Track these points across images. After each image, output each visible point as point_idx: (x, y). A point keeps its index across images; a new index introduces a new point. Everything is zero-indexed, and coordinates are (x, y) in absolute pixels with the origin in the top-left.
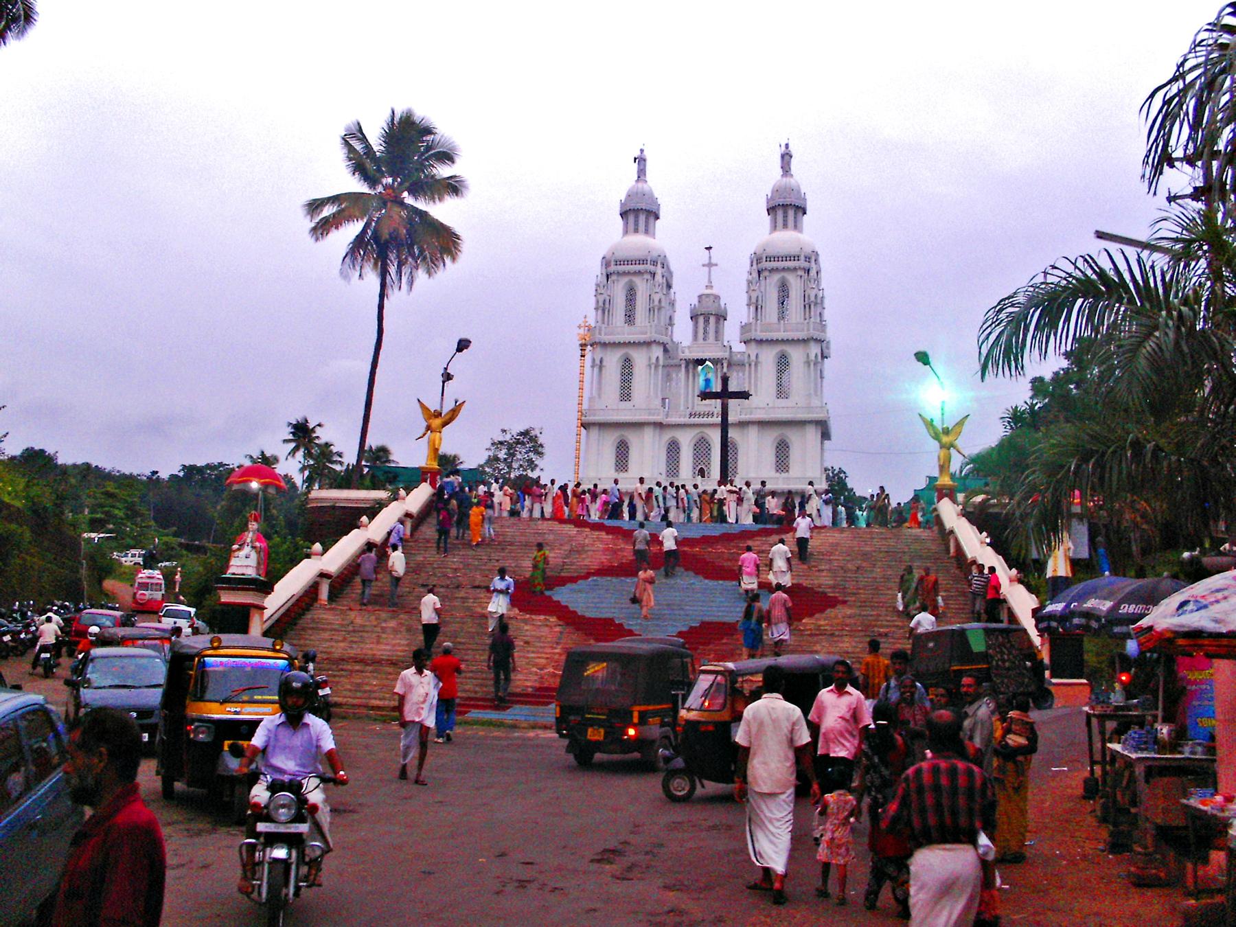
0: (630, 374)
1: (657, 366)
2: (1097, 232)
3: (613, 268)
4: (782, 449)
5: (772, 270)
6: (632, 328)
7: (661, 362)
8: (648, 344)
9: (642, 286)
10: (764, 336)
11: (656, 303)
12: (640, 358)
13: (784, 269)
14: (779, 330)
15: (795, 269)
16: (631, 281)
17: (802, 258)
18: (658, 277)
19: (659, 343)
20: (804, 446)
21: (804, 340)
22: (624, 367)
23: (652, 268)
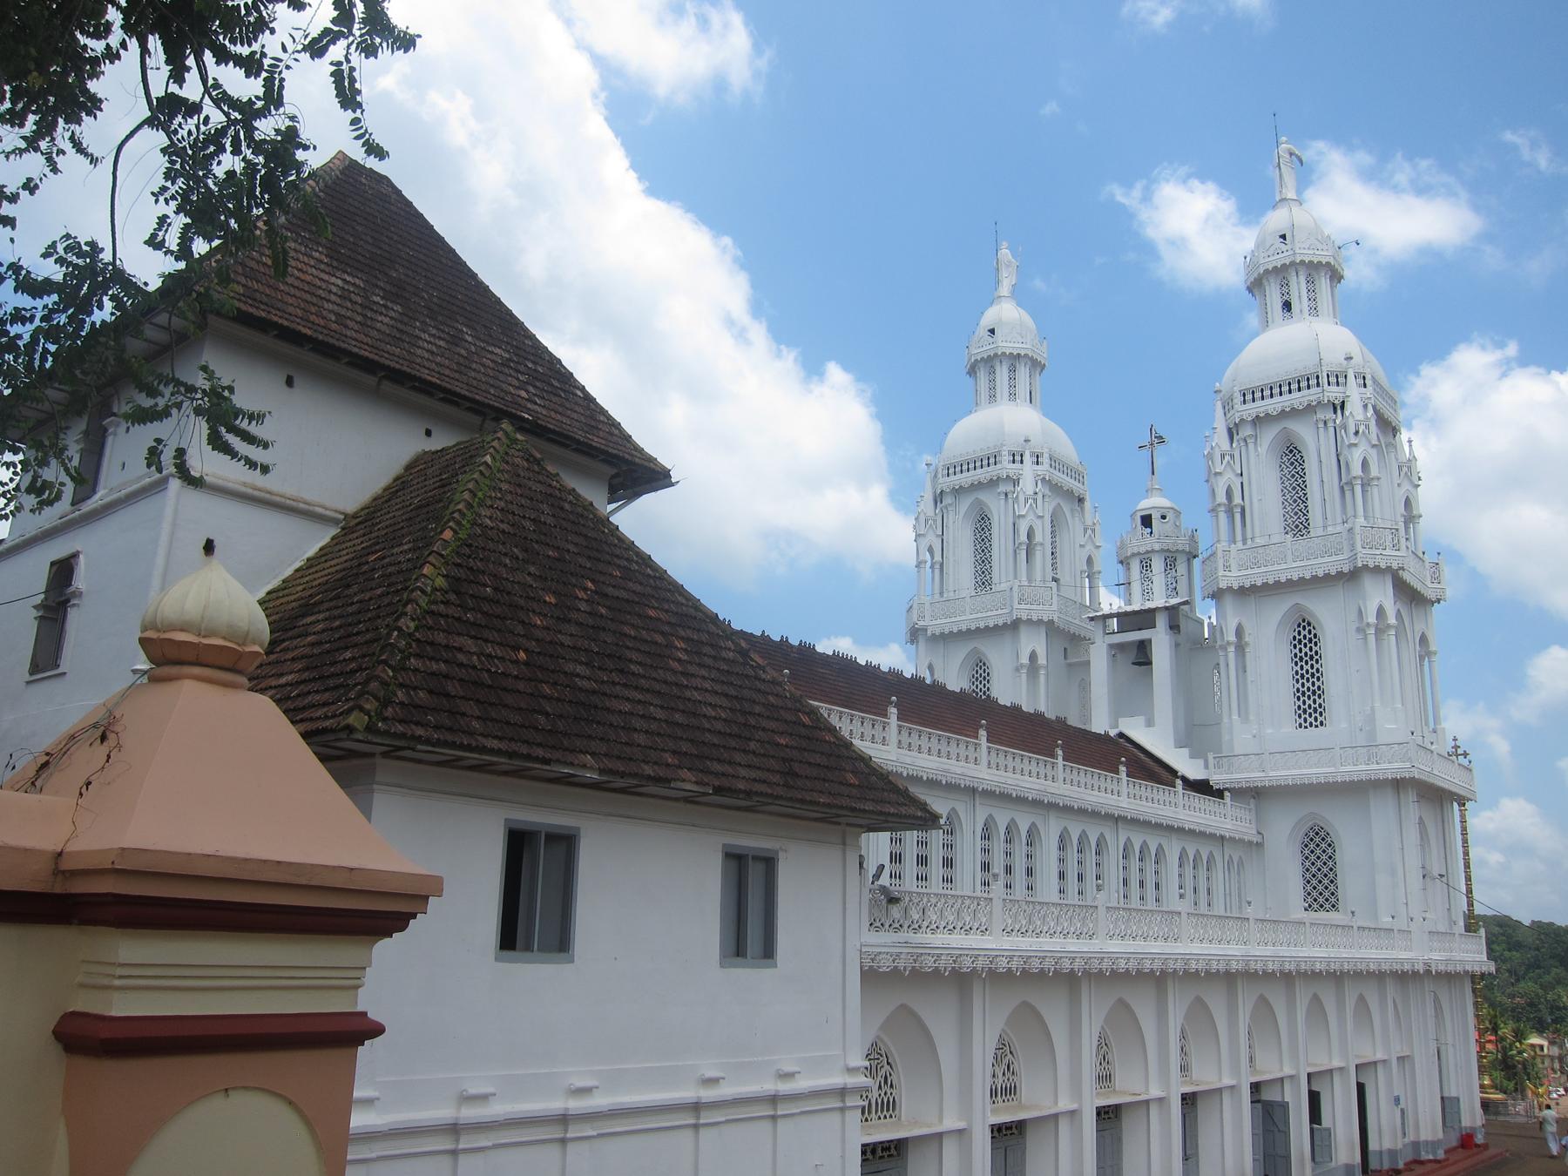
0: (1315, 657)
1: (1380, 631)
2: (35, 668)
3: (946, 483)
4: (1319, 856)
5: (1258, 421)
6: (1302, 544)
7: (1042, 660)
8: (1351, 577)
9: (1314, 441)
10: (1256, 576)
11: (1357, 470)
12: (1330, 615)
13: (1284, 414)
14: (964, 612)
15: (1310, 409)
16: (979, 503)
17: (1006, 458)
18: (1356, 410)
19: (1377, 570)
20: (1376, 848)
21: (1340, 575)
22: (1296, 642)
23: (1333, 393)
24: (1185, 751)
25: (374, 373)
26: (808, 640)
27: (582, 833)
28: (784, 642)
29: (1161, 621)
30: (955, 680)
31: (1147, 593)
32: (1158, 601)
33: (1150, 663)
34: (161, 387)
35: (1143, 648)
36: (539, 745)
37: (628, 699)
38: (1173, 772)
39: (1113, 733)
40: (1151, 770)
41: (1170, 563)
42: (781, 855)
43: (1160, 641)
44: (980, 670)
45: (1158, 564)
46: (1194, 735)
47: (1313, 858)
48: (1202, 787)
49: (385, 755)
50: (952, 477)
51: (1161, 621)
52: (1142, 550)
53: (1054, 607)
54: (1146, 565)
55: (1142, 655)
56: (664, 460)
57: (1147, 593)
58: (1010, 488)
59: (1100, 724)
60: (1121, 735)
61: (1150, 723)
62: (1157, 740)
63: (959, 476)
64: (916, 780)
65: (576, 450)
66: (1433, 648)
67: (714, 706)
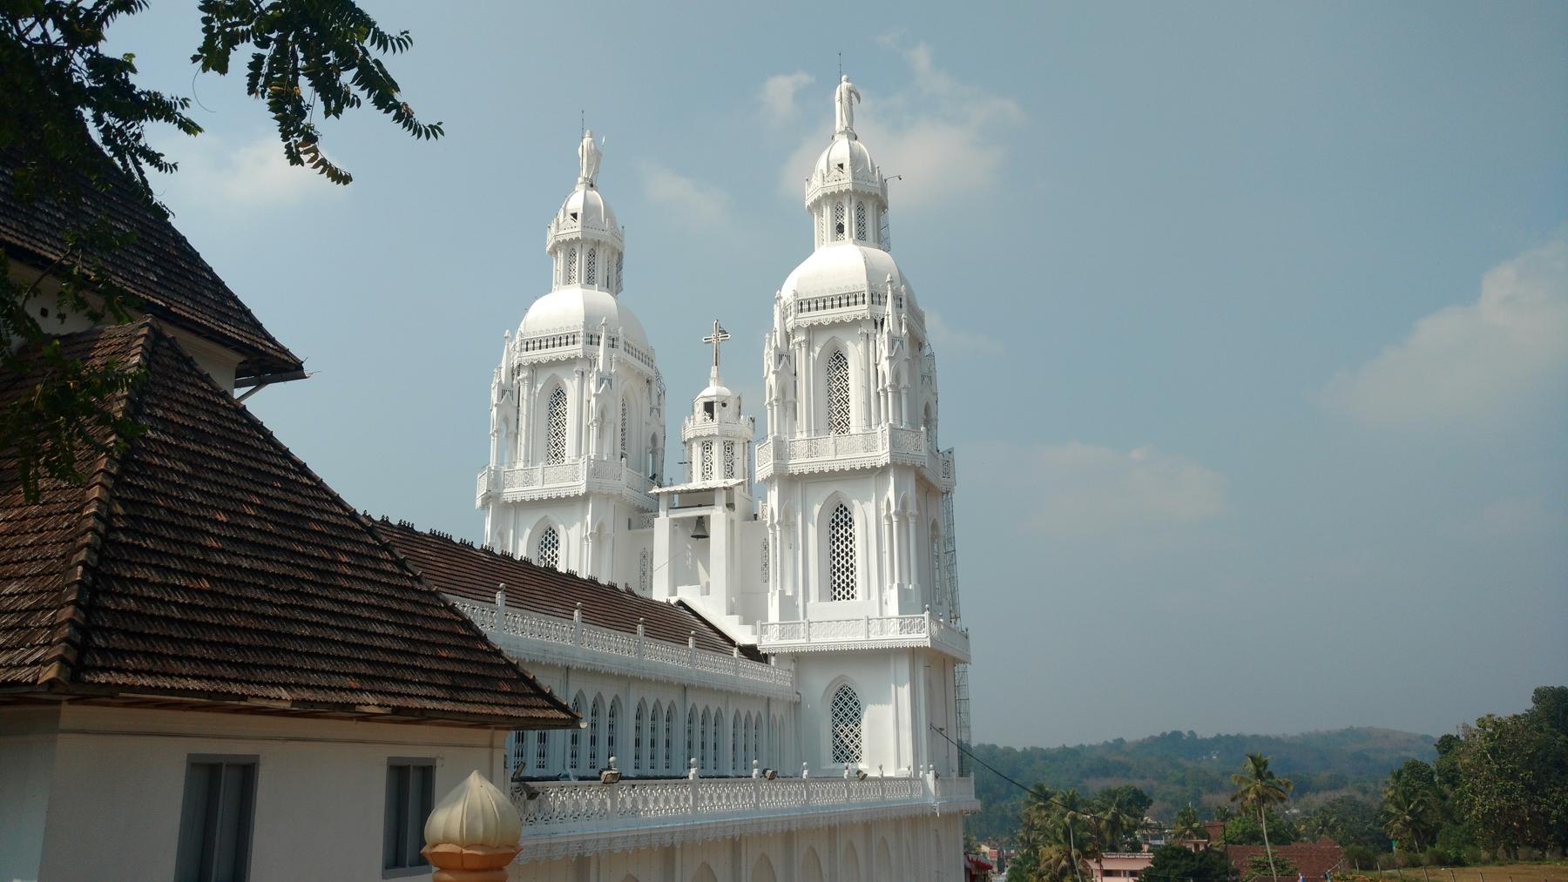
16: (554, 378)
24: (736, 618)
25: (36, 266)
26: (408, 519)
27: (262, 761)
28: (385, 522)
29: (721, 499)
30: (522, 547)
31: (706, 472)
32: (717, 481)
33: (707, 537)
34: (41, 406)
35: (702, 522)
36: (236, 681)
37: (307, 622)
38: (732, 642)
39: (673, 600)
40: (717, 640)
41: (729, 447)
42: (439, 763)
43: (718, 517)
44: (549, 539)
45: (716, 448)
46: (748, 605)
47: (841, 715)
48: (750, 652)
49: (71, 702)
50: (531, 352)
51: (721, 499)
52: (705, 433)
53: (624, 481)
54: (707, 446)
55: (700, 529)
56: (297, 352)
57: (706, 472)
58: (586, 367)
59: (660, 593)
60: (680, 603)
61: (706, 591)
62: (712, 606)
63: (537, 351)
64: (533, 663)
65: (208, 338)
66: (261, 105)
67: (381, 622)
